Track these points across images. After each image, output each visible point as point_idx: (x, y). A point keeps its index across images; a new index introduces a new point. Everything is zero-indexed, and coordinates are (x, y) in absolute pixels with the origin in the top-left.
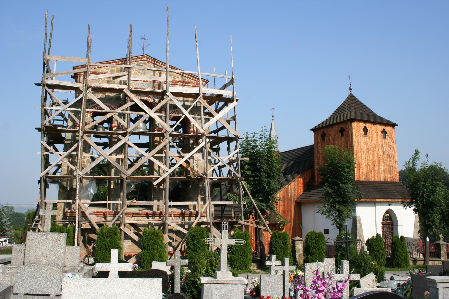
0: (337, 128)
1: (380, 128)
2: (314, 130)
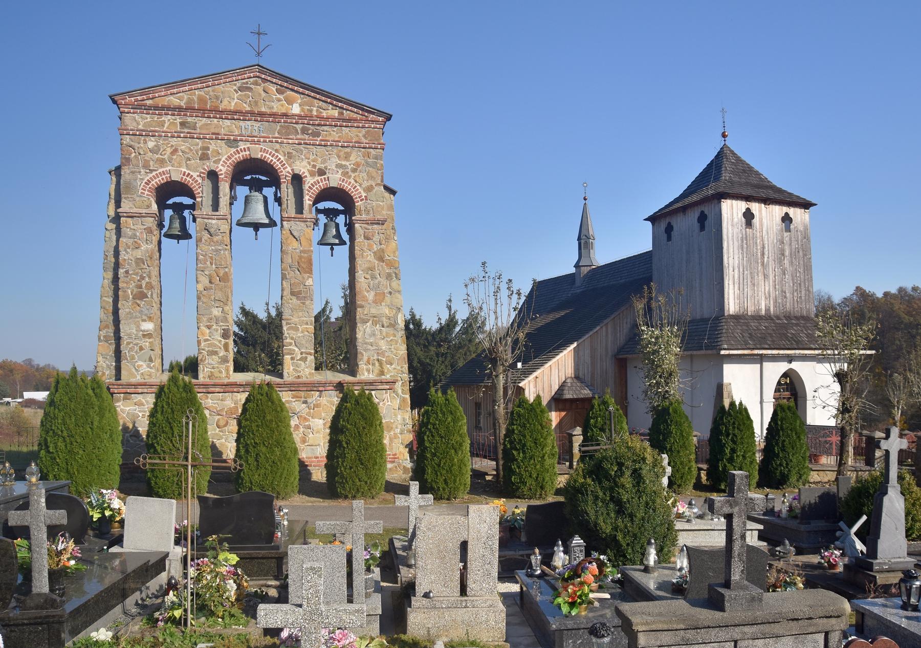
0: (693, 215)
1: (778, 211)
2: (653, 219)
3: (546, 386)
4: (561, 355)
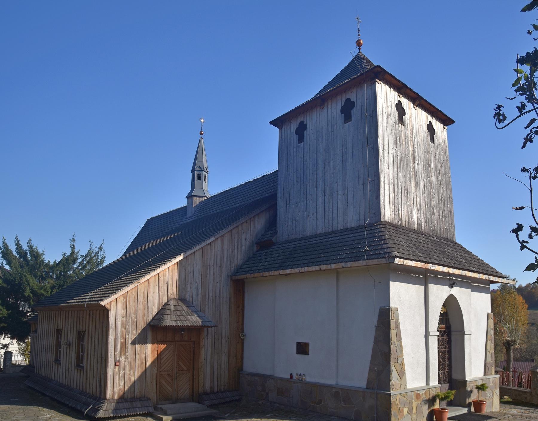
0: (334, 109)
2: (278, 122)
3: (141, 307)
4: (164, 267)
